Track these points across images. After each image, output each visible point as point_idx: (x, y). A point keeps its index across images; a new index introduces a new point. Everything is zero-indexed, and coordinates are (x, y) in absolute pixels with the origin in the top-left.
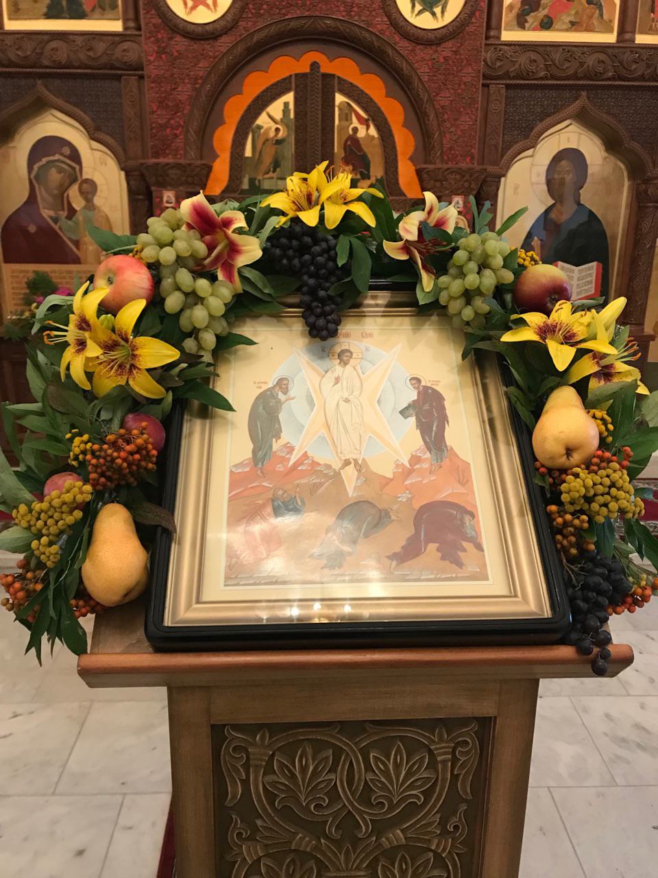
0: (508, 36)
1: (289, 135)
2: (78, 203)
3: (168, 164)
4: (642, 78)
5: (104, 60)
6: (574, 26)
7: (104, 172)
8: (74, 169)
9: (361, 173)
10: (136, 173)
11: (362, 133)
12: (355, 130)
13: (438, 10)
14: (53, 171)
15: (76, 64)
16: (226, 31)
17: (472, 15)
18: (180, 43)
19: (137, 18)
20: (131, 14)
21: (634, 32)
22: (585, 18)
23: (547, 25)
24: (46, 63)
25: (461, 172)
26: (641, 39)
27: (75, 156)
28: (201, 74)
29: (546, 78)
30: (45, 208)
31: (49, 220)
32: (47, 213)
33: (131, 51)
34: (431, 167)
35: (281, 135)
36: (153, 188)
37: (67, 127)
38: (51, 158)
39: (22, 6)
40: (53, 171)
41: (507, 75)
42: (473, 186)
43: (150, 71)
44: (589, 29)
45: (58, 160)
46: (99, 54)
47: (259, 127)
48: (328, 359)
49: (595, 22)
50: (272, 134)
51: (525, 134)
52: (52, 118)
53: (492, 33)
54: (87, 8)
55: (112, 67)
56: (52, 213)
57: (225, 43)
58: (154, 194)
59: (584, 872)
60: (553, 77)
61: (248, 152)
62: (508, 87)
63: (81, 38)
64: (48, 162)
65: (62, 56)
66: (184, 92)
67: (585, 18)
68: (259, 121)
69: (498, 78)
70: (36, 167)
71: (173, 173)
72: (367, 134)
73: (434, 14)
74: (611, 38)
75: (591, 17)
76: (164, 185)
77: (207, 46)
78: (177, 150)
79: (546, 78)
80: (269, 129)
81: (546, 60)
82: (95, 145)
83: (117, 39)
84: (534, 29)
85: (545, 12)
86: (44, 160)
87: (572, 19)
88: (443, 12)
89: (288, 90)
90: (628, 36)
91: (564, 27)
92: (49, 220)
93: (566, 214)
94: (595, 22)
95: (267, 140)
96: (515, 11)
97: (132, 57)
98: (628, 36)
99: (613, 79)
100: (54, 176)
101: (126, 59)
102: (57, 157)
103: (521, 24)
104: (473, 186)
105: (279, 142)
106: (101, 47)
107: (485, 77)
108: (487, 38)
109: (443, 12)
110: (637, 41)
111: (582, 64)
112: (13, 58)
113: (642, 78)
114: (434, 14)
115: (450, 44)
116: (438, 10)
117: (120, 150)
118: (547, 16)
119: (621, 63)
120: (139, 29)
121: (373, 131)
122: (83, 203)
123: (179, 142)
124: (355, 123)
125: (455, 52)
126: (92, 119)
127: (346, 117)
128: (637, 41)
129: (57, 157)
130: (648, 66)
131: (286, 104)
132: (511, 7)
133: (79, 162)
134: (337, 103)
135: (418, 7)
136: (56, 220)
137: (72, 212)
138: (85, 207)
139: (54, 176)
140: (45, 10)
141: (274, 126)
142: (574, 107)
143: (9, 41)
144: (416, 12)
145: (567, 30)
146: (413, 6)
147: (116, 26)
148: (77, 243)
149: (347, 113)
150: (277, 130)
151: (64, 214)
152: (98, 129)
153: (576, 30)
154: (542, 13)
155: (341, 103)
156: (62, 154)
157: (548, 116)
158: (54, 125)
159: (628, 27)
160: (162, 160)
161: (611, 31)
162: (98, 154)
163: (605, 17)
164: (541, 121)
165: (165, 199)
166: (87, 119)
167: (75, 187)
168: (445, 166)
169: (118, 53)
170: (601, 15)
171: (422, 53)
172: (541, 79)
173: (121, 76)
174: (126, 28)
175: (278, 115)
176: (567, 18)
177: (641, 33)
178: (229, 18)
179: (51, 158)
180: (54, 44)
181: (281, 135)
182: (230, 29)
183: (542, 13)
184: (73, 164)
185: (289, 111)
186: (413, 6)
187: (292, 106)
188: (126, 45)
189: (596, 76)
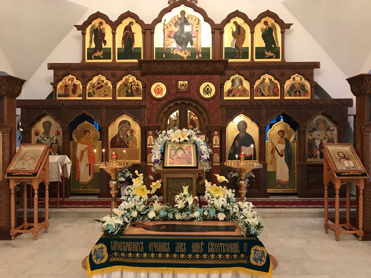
0: (225, 98)
1: (178, 119)
2: (129, 134)
3: (150, 126)
4: (256, 106)
5: (138, 105)
6: (240, 96)
7: (136, 128)
8: (129, 127)
9: (194, 127)
10: (143, 128)
11: (194, 118)
12: (192, 118)
13: (209, 94)
14: (124, 127)
15: (71, 106)
16: (164, 99)
17: (217, 95)
18: (154, 102)
19: (145, 97)
20: (144, 96)
21: (254, 97)
22: (242, 94)
23: (234, 96)
24: (126, 106)
25: (216, 126)
26: (255, 98)
27: (129, 124)
28: (159, 107)
29: (234, 106)
30: (121, 135)
31: (122, 138)
32: (122, 137)
33: (143, 103)
34: (209, 125)
35: (176, 119)
36: (147, 131)
37: (128, 118)
38: (124, 125)
39: (121, 94)
40: (124, 127)
41: (225, 106)
42: (219, 129)
43: (148, 107)
44: (243, 96)
45: (126, 125)
46: (137, 104)
47: (171, 118)
48: (26, 235)
49: (245, 95)
50: (174, 119)
51: (231, 118)
52: (125, 116)
53: (222, 98)
54: (135, 95)
55: (140, 106)
56: (123, 137)
57: (163, 102)
58: (147, 132)
59: (349, 164)
60: (282, 106)
61: (168, 123)
62: (226, 108)
63: (133, 101)
64: (123, 126)
65: (129, 105)
66: (155, 111)
67: (242, 94)
68: (171, 116)
69: (223, 107)
70: (120, 127)
71: (152, 128)
72: (195, 118)
73: (208, 95)
74: (249, 98)
75: (244, 94)
76: (149, 130)
77: (160, 102)
78: (153, 123)
79: (234, 106)
80: (173, 118)
81: (234, 103)
82: (134, 122)
83: (141, 101)
84: (231, 97)
85: (233, 93)
86: (122, 125)
87: (239, 94)
88: (210, 94)
89: (177, 110)
90: (252, 98)
91: (238, 96)
92: (122, 138)
93: (242, 136)
94: (245, 95)
95: (173, 120)
96: (226, 94)
97: (144, 104)
98: (252, 98)
99: (249, 106)
100: (124, 129)
101: (143, 105)
102: (125, 124)
103: (228, 96)
104: (219, 129)
105: (175, 121)
106: (122, 103)
107: (220, 107)
108: (220, 99)
109: (210, 94)
110: (254, 99)
111: (273, 103)
112: (119, 105)
113: (256, 106)
114: (208, 95)
115: (212, 100)
116: (209, 94)
117: (140, 123)
118: (234, 94)
119: (266, 103)
120: (146, 99)
121: (196, 118)
122: (130, 134)
123: (153, 121)
124: (192, 116)
125: (214, 102)
126: (134, 117)
127: (190, 115)
128: (254, 99)
129: (125, 124)
130: (257, 104)
131: (177, 113)
132: (226, 92)
133: (130, 125)
134: (188, 112)
135: (205, 94)
136: (123, 138)
137: (127, 136)
138: (131, 135)
139: (124, 129)
140: (126, 95)
141: (174, 117)
142: (242, 112)
143: (87, 101)
144: (205, 94)
145: (239, 97)
146: (204, 94)
147: (141, 98)
148: (128, 143)
149: (190, 114)
150: (175, 118)
151: (126, 137)
152: (135, 119)
153: (240, 97)
154: (233, 94)
155: (189, 112)
156: (126, 124)
157: (237, 114)
158: (125, 118)
159: (252, 96)
160: (149, 125)
161: (249, 96)
162: (134, 124)
163: (247, 94)
164: (234, 115)
165: (150, 133)
166: (133, 117)
167: (129, 131)
168: (213, 125)
169: (141, 104)
170: (246, 93)
171: (206, 102)
172: (279, 106)
173: (141, 108)
174: (113, 99)
175: (175, 115)
176: (238, 94)
177: (256, 96)
178: (165, 97)
179: (124, 125)
180: (37, 102)
181: (176, 119)
182: (165, 99)
183: (233, 94)
184: (129, 126)
185: (178, 114)
186: (204, 94)
187: (178, 113)
188: (143, 102)
189: (245, 106)
